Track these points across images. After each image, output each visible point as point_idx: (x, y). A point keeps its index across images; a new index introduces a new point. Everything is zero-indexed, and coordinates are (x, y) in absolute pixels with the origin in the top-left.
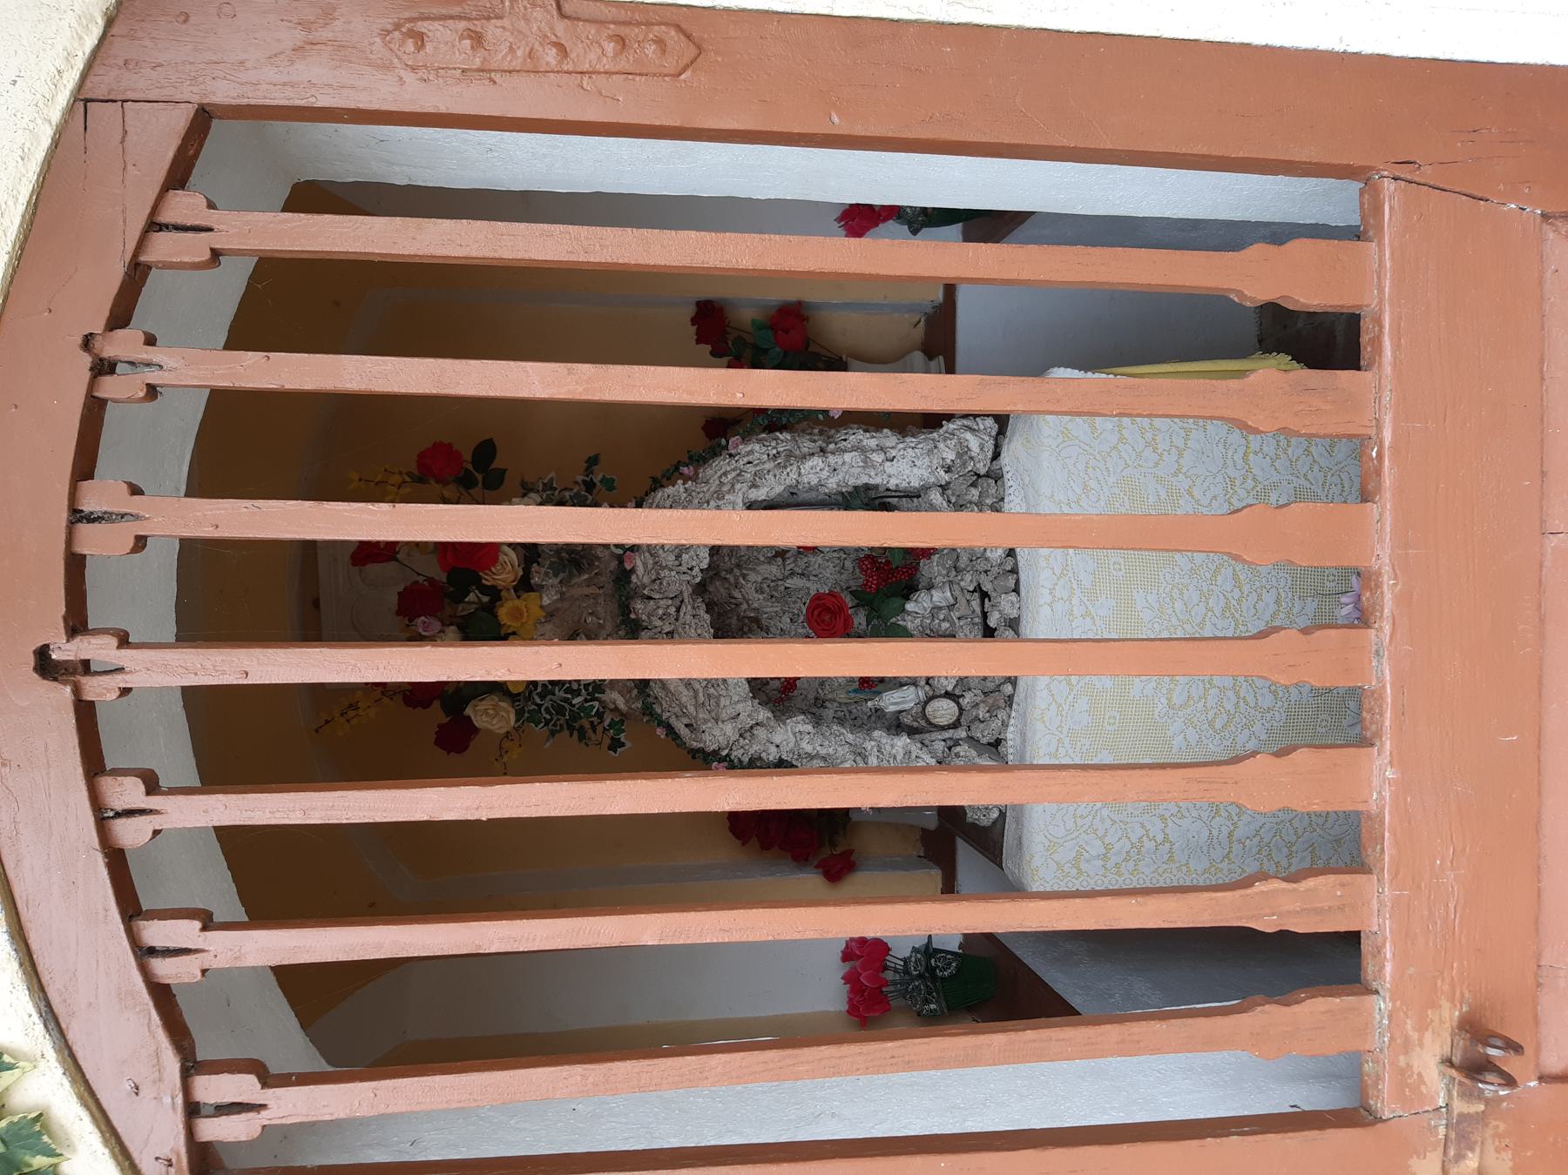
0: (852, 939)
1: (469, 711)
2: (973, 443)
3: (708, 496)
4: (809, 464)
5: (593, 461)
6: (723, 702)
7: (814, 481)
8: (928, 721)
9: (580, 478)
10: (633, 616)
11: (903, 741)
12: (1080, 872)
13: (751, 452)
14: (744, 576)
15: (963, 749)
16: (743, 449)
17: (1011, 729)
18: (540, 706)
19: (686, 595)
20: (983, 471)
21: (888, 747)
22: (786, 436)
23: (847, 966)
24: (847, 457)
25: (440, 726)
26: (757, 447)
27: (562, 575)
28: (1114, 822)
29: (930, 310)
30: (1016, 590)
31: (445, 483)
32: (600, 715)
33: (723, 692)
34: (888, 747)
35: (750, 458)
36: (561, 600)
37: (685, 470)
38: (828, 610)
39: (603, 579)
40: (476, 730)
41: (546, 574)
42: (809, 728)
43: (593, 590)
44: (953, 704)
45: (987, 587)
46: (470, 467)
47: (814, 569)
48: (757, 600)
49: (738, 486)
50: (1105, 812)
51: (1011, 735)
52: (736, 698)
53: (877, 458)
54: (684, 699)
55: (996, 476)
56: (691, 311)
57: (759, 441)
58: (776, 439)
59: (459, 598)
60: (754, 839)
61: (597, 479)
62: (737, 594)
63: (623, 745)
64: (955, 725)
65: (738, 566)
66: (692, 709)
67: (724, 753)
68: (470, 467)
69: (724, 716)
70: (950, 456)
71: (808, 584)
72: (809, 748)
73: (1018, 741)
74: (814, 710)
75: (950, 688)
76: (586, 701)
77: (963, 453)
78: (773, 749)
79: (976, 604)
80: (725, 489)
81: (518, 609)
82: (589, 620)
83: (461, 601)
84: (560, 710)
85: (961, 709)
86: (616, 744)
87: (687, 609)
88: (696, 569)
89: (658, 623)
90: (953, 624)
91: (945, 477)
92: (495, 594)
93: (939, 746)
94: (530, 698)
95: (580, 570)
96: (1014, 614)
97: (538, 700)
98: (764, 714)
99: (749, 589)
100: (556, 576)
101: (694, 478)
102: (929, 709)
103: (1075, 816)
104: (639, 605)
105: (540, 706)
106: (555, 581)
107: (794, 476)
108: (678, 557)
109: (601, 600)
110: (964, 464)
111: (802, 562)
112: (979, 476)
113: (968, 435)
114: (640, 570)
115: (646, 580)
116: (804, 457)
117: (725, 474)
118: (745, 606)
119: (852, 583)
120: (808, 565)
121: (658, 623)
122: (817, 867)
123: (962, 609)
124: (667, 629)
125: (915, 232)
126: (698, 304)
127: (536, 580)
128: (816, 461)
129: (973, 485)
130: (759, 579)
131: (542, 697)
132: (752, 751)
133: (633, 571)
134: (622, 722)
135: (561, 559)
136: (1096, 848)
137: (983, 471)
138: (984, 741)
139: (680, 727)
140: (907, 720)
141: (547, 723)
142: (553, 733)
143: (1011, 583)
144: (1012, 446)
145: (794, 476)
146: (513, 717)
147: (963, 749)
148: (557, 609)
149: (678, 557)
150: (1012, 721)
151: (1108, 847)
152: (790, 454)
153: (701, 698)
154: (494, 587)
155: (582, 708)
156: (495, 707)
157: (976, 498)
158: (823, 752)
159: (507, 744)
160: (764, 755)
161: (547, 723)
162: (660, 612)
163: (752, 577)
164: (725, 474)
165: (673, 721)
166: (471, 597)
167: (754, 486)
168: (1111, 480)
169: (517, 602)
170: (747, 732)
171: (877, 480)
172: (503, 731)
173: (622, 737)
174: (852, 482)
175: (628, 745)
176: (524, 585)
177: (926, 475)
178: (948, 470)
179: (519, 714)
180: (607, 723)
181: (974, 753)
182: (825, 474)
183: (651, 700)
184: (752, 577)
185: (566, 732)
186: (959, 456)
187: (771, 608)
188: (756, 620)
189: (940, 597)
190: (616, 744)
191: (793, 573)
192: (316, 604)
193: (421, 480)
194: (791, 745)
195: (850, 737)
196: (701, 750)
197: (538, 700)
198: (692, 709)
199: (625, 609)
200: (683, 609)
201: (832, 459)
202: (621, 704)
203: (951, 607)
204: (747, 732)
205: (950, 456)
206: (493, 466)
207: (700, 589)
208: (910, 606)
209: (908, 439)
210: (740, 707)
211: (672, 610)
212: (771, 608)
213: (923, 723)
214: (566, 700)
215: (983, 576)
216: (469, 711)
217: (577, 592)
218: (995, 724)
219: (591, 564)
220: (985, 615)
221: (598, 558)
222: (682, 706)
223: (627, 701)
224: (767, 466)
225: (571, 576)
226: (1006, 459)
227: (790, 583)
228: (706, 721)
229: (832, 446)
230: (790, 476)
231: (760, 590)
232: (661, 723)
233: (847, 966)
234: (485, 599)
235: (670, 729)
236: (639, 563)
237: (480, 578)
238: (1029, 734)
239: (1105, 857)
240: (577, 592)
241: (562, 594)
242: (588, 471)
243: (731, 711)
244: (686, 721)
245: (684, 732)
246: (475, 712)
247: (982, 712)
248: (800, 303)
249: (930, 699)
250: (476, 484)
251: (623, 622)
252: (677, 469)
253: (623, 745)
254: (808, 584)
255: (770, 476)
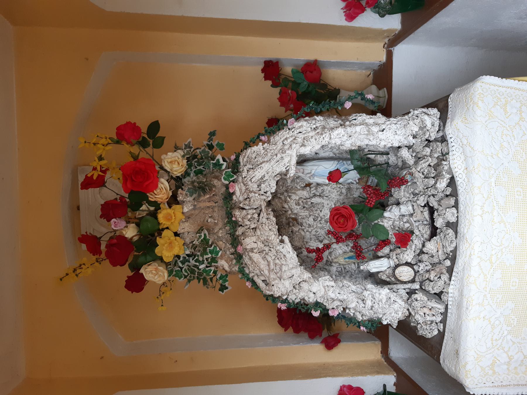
0: (344, 386)
1: (142, 271)
2: (428, 122)
3: (276, 152)
4: (336, 132)
5: (212, 134)
6: (284, 268)
7: (339, 143)
8: (396, 278)
9: (205, 142)
10: (234, 219)
11: (385, 291)
12: (494, 373)
13: (300, 127)
14: (290, 197)
15: (419, 296)
16: (297, 124)
17: (451, 287)
18: (181, 268)
19: (263, 207)
20: (432, 139)
21: (377, 295)
22: (320, 118)
23: (291, 329)
24: (358, 128)
25: (128, 277)
26: (304, 123)
27: (194, 196)
28: (514, 343)
29: (376, 68)
30: (456, 206)
31: (133, 145)
32: (215, 272)
33: (284, 263)
34: (377, 295)
35: (301, 130)
36: (194, 209)
37: (263, 138)
38: (343, 216)
39: (217, 198)
40: (145, 280)
41: (186, 195)
42: (332, 283)
43: (212, 204)
44: (410, 269)
45: (433, 203)
46: (146, 136)
47: (326, 193)
48: (296, 209)
49: (294, 146)
50: (509, 337)
51: (452, 290)
52: (291, 266)
53: (375, 129)
54: (262, 266)
55: (443, 140)
56: (262, 66)
57: (306, 121)
58: (316, 119)
59: (136, 207)
60: (291, 328)
61: (215, 143)
62: (286, 206)
63: (227, 288)
64: (413, 281)
65: (286, 191)
66: (266, 272)
67: (284, 297)
68: (146, 136)
69: (285, 276)
70: (416, 129)
71: (323, 201)
72: (333, 296)
73: (456, 294)
74: (327, 267)
75: (409, 261)
76: (207, 267)
77: (423, 128)
78: (312, 295)
79: (426, 214)
80: (286, 147)
81: (169, 214)
82: (209, 220)
83: (138, 209)
84: (193, 272)
85: (416, 272)
86: (223, 288)
87: (264, 215)
88: (269, 193)
89: (248, 223)
90: (411, 225)
91: (412, 141)
92: (157, 206)
93: (403, 293)
94: (176, 263)
95: (205, 192)
96: (453, 220)
97: (180, 265)
98: (307, 275)
99: (292, 204)
100: (191, 196)
101: (269, 142)
102: (397, 271)
103: (492, 340)
104: (237, 213)
105: (181, 268)
106: (189, 199)
107: (327, 139)
108: (259, 186)
109: (216, 209)
110: (424, 134)
111: (320, 190)
112: (429, 141)
113: (426, 117)
114: (238, 193)
115: (241, 199)
116: (332, 129)
117: (286, 139)
118: (290, 212)
119: (346, 201)
120: (323, 191)
121: (248, 223)
122: (322, 342)
123: (418, 216)
124: (253, 226)
125: (382, 16)
126: (266, 62)
127: (180, 198)
128: (341, 130)
129: (426, 146)
130: (297, 198)
131: (183, 263)
132: (300, 296)
133: (233, 193)
134: (227, 275)
135: (194, 187)
136: (504, 358)
137: (432, 139)
138: (433, 292)
139: (259, 281)
140: (384, 277)
141: (186, 277)
142: (189, 281)
143: (452, 201)
144: (455, 122)
145: (327, 139)
146: (166, 275)
147: (419, 296)
148: (192, 214)
149: (259, 186)
150: (452, 282)
151: (510, 358)
152: (324, 128)
153: (272, 266)
154: (155, 202)
155: (204, 270)
156: (156, 269)
157: (428, 154)
158: (341, 297)
159: (163, 289)
160: (306, 298)
161: (186, 277)
162: (249, 217)
163: (294, 197)
164: (286, 139)
165: (255, 279)
166: (144, 207)
167: (303, 145)
168: (516, 142)
169: (169, 211)
170: (297, 286)
171: (374, 142)
172: (161, 282)
173: (227, 284)
174: (359, 143)
175: (230, 288)
176: (173, 201)
177: (403, 139)
178: (414, 137)
179: (170, 273)
180: (218, 276)
181: (426, 299)
182: (345, 138)
183: (243, 265)
184: (294, 197)
185: (196, 281)
186: (421, 128)
187: (304, 213)
188: (295, 219)
189: (406, 209)
190: (223, 288)
191: (315, 195)
192: (78, 208)
193: (117, 142)
194: (322, 293)
195: (354, 288)
196: (272, 296)
197: (180, 265)
198: (266, 272)
199: (229, 215)
200: (262, 215)
201: (349, 129)
202: (227, 267)
203: (411, 215)
204: (297, 286)
205: (416, 129)
206: (158, 135)
207: (269, 203)
208: (386, 214)
209: (392, 119)
210: (294, 271)
211: (256, 216)
212: (304, 213)
213: (393, 279)
214: (195, 266)
215: (432, 197)
216: (142, 271)
217: (202, 205)
218: (441, 283)
219: (211, 190)
220: (432, 220)
221: (215, 186)
222: (261, 270)
223: (230, 266)
224: (311, 134)
225: (199, 196)
226: (450, 130)
227: (314, 200)
228: (274, 279)
229: (348, 123)
230: (325, 139)
231: (298, 204)
232: (248, 279)
233: (291, 329)
234: (152, 209)
235: (254, 283)
236: (237, 189)
237: (148, 197)
238: (465, 292)
239: (508, 363)
240: (202, 205)
241: (195, 206)
242: (210, 139)
243: (289, 274)
244: (263, 278)
245: (262, 285)
246: (146, 272)
247: (432, 276)
248: (316, 61)
249: (397, 266)
250: (149, 145)
251: (228, 222)
252: (258, 137)
253: (227, 288)
254: (323, 201)
255: (313, 140)
